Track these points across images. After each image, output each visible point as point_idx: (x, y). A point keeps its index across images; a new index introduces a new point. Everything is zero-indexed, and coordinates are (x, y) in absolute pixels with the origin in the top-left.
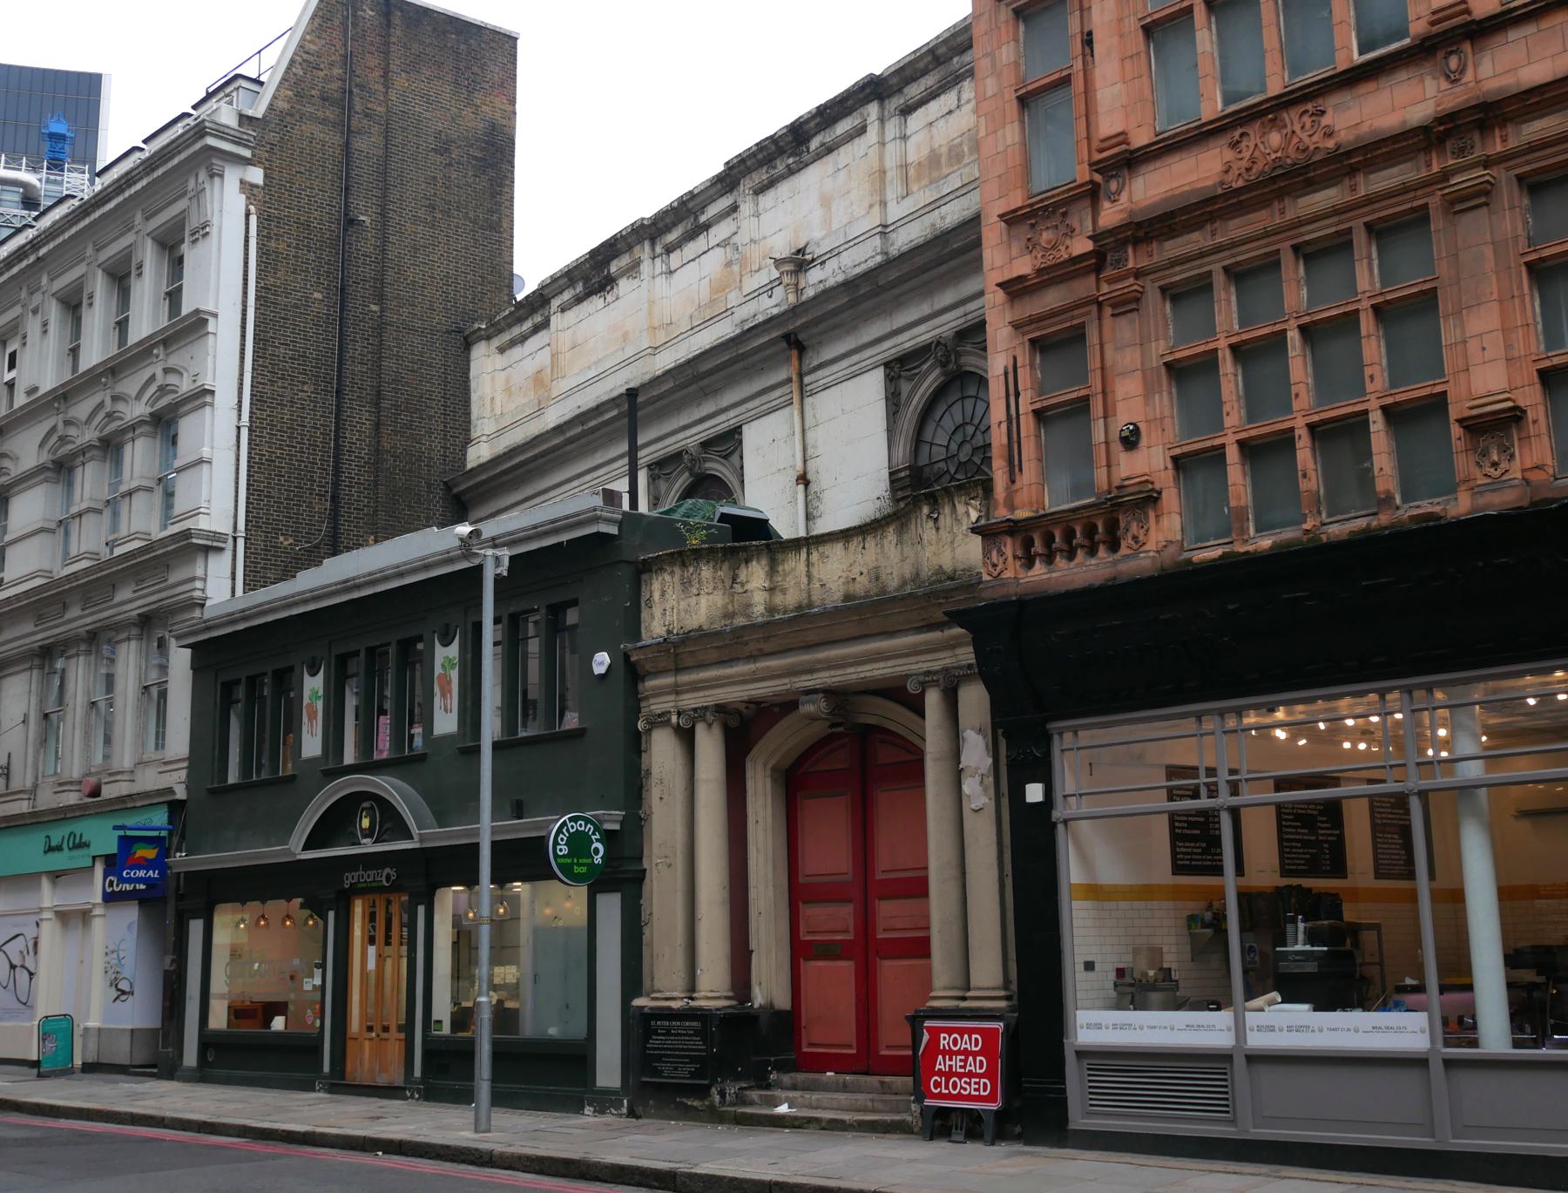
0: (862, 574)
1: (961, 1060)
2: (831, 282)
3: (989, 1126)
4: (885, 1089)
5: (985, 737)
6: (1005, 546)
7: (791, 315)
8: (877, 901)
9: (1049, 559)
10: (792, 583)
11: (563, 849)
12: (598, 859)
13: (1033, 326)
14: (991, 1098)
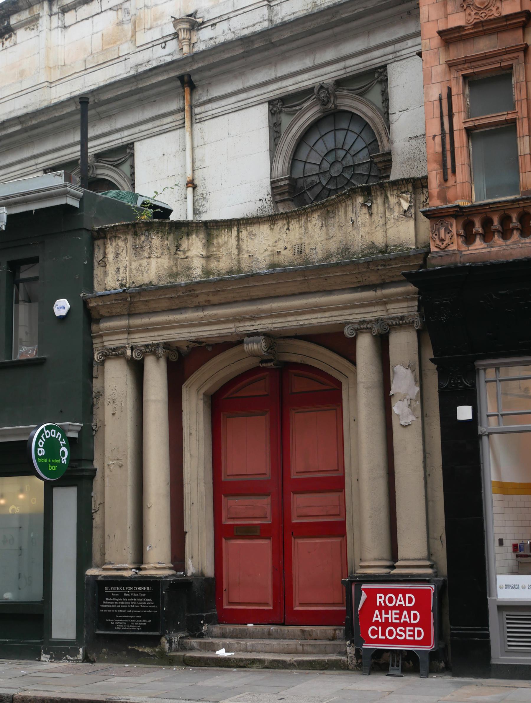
0: (286, 248)
1: (396, 614)
2: (221, 39)
3: (424, 663)
4: (305, 635)
5: (413, 371)
6: (451, 226)
7: (190, 60)
8: (292, 494)
9: (487, 237)
10: (225, 254)
11: (42, 452)
12: (64, 460)
13: (466, 65)
14: (426, 641)
